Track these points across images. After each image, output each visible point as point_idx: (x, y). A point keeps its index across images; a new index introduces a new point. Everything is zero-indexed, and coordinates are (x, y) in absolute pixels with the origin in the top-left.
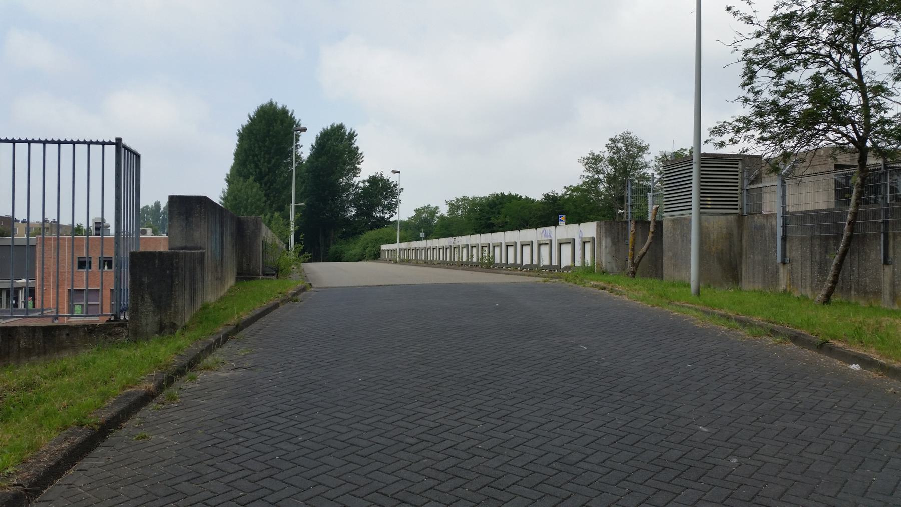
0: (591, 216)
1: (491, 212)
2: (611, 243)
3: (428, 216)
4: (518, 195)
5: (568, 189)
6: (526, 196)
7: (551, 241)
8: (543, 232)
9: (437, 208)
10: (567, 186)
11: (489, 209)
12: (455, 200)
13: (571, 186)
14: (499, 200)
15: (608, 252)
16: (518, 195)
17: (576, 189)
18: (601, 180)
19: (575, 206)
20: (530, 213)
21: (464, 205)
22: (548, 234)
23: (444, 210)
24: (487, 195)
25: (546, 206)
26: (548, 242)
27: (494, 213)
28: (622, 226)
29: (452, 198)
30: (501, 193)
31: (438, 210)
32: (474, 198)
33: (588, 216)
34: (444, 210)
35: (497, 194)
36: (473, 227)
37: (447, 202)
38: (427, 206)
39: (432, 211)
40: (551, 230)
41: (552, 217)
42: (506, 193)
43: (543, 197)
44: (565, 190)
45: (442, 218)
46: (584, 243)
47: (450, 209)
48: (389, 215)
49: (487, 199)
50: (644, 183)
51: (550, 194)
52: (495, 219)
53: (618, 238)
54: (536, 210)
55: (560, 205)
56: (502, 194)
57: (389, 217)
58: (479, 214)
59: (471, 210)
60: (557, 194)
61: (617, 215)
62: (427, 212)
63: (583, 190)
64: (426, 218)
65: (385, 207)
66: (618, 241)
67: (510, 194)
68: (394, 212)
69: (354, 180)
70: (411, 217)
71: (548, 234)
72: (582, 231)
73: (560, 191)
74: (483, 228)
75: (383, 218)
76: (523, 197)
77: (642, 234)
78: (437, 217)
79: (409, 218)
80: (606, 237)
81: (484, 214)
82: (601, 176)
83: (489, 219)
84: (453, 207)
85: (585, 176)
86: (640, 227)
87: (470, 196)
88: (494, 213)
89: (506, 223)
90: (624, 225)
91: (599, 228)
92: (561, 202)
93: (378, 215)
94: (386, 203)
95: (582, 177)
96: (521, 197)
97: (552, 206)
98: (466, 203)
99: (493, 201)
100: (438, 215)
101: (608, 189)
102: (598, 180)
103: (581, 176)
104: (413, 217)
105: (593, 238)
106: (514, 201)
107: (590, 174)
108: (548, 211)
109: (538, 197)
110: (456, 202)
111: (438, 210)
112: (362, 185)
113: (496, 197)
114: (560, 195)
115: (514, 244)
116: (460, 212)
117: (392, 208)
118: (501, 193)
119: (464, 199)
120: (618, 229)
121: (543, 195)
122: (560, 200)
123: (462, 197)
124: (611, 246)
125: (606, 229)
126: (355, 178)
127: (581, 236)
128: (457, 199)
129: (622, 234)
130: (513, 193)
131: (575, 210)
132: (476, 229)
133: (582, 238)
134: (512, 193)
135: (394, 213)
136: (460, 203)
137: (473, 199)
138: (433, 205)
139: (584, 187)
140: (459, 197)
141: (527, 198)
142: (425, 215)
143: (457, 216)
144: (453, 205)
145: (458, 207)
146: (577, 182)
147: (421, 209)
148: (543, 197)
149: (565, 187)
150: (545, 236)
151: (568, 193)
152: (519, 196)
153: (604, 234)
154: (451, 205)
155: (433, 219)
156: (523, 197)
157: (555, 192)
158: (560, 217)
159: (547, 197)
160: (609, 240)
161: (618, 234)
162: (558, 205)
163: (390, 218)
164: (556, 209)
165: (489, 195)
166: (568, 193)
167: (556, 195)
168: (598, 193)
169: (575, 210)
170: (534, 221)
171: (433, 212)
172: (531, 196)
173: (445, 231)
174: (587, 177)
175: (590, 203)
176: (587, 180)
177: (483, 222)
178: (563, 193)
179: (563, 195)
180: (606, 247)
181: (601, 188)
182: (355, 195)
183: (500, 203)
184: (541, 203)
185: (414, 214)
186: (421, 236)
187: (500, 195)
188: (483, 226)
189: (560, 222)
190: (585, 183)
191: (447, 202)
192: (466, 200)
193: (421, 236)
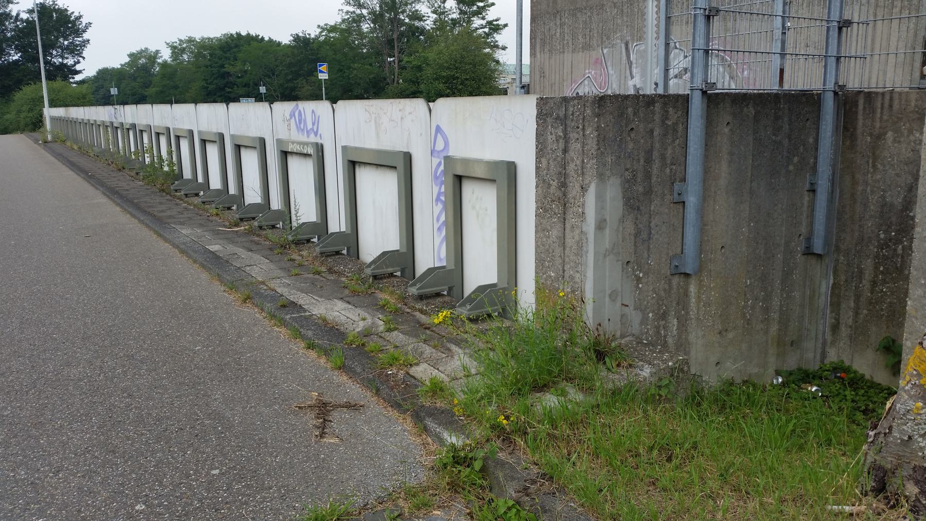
0: (356, 65)
1: (226, 58)
2: (619, 204)
3: (146, 63)
4: (259, 35)
5: (323, 29)
6: (270, 38)
7: (320, 149)
8: (292, 115)
9: (157, 52)
10: (322, 24)
11: (221, 53)
12: (178, 42)
13: (326, 25)
14: (235, 42)
15: (607, 245)
16: (259, 35)
17: (333, 29)
18: (364, 17)
19: (335, 51)
20: (276, 60)
21: (190, 48)
22: (310, 126)
23: (166, 55)
24: (218, 35)
25: (296, 51)
26: (310, 150)
27: (229, 59)
28: (665, 117)
29: (174, 39)
30: (237, 33)
31: (160, 55)
32: (203, 39)
33: (352, 65)
34: (166, 55)
35: (231, 34)
36: (203, 77)
37: (168, 44)
38: (143, 49)
39: (151, 56)
40: (318, 113)
41: (306, 65)
42: (244, 33)
43: (292, 38)
44: (320, 30)
45: (165, 65)
46: (459, 179)
47: (172, 53)
48: (72, 60)
49: (219, 40)
50: (417, 23)
51: (301, 35)
52: (231, 67)
53: (648, 176)
54: (283, 56)
55: (314, 50)
56: (239, 34)
57: (73, 63)
58: (209, 60)
59: (198, 55)
60: (309, 35)
61: (387, 63)
62: (145, 57)
63: (342, 31)
64: (143, 65)
65: (65, 49)
66: (649, 192)
67: (248, 34)
68: (81, 57)
69: (9, 9)
70: (123, 63)
71: (310, 126)
72: (443, 127)
73: (313, 32)
74: (216, 78)
75: (65, 65)
76: (267, 39)
77: (731, 154)
78: (159, 64)
79: (121, 65)
80: (601, 177)
81: (216, 60)
82: (365, 12)
83: (222, 66)
84: (177, 51)
85: (345, 11)
86: (729, 118)
87: (198, 36)
88: (229, 59)
89: (246, 72)
90: (674, 115)
91: (554, 133)
92: (315, 46)
93: (55, 61)
94: (66, 43)
95: (341, 12)
96: (263, 38)
97: (304, 51)
98: (193, 45)
99: (226, 42)
100: (160, 61)
101: (373, 30)
102: (361, 16)
103: (339, 10)
104: (126, 63)
105: (511, 169)
106: (254, 44)
107: (351, 9)
108: (299, 58)
109: (285, 39)
110: (180, 45)
111: (160, 55)
112: (24, 16)
113: (230, 38)
114: (313, 36)
115: (217, 140)
116: (185, 57)
117: (76, 50)
118: (237, 33)
119: (191, 40)
120: (652, 131)
121: (291, 35)
122: (313, 43)
123: (187, 38)
124: (622, 220)
125: (602, 139)
126: (10, 5)
127: (440, 145)
128: (181, 41)
129: (663, 157)
130: (253, 33)
131: (334, 56)
132: (207, 80)
133: (449, 160)
134: (251, 33)
135: (81, 59)
136: (185, 45)
137: (202, 40)
138: (153, 49)
139: (343, 26)
140: (183, 38)
141: (271, 40)
142: (142, 61)
143: (182, 63)
144: (175, 48)
145: (183, 51)
146: (334, 18)
147: (137, 54)
148: (292, 38)
149: (319, 26)
150: (299, 129)
151: (324, 34)
152: (260, 37)
153: (591, 164)
154: (173, 48)
155: (153, 66)
156: (267, 39)
157: (307, 32)
158: (320, 66)
159: (297, 38)
160: (613, 190)
161: (649, 161)
162: (311, 50)
163: (75, 65)
164: (309, 54)
165: (220, 35)
166: (324, 34)
167: (308, 36)
168: (361, 34)
169: (334, 56)
170: (282, 70)
171: (152, 57)
172: (277, 38)
173: (168, 82)
174: (347, 12)
175: (352, 48)
176: (346, 17)
177: (215, 70)
178: (317, 33)
179: (317, 37)
180: (600, 226)
181: (366, 27)
182: (14, 30)
183: (237, 46)
184: (288, 47)
185: (127, 59)
186: (112, 93)
187: (235, 36)
188: (215, 76)
189: (320, 74)
190: (344, 21)
191: (168, 44)
192: (193, 41)
193: (112, 93)
